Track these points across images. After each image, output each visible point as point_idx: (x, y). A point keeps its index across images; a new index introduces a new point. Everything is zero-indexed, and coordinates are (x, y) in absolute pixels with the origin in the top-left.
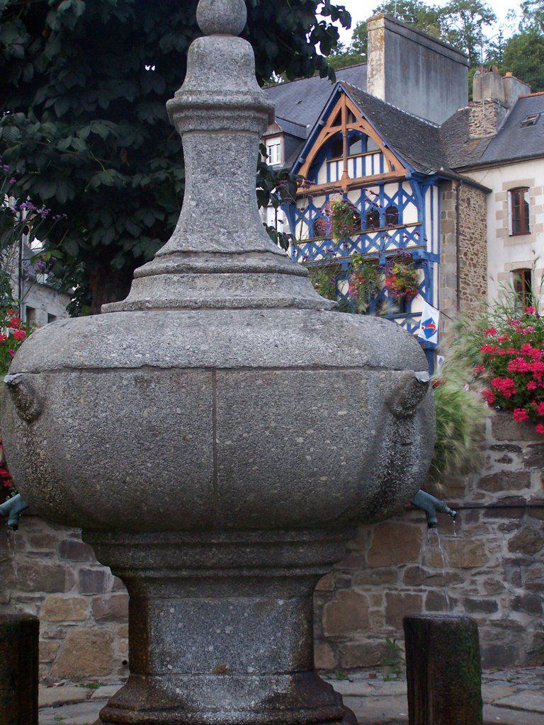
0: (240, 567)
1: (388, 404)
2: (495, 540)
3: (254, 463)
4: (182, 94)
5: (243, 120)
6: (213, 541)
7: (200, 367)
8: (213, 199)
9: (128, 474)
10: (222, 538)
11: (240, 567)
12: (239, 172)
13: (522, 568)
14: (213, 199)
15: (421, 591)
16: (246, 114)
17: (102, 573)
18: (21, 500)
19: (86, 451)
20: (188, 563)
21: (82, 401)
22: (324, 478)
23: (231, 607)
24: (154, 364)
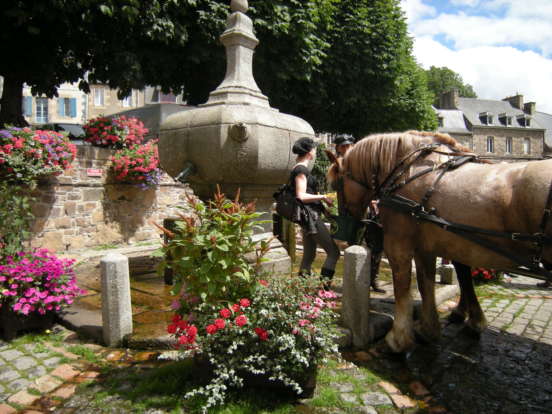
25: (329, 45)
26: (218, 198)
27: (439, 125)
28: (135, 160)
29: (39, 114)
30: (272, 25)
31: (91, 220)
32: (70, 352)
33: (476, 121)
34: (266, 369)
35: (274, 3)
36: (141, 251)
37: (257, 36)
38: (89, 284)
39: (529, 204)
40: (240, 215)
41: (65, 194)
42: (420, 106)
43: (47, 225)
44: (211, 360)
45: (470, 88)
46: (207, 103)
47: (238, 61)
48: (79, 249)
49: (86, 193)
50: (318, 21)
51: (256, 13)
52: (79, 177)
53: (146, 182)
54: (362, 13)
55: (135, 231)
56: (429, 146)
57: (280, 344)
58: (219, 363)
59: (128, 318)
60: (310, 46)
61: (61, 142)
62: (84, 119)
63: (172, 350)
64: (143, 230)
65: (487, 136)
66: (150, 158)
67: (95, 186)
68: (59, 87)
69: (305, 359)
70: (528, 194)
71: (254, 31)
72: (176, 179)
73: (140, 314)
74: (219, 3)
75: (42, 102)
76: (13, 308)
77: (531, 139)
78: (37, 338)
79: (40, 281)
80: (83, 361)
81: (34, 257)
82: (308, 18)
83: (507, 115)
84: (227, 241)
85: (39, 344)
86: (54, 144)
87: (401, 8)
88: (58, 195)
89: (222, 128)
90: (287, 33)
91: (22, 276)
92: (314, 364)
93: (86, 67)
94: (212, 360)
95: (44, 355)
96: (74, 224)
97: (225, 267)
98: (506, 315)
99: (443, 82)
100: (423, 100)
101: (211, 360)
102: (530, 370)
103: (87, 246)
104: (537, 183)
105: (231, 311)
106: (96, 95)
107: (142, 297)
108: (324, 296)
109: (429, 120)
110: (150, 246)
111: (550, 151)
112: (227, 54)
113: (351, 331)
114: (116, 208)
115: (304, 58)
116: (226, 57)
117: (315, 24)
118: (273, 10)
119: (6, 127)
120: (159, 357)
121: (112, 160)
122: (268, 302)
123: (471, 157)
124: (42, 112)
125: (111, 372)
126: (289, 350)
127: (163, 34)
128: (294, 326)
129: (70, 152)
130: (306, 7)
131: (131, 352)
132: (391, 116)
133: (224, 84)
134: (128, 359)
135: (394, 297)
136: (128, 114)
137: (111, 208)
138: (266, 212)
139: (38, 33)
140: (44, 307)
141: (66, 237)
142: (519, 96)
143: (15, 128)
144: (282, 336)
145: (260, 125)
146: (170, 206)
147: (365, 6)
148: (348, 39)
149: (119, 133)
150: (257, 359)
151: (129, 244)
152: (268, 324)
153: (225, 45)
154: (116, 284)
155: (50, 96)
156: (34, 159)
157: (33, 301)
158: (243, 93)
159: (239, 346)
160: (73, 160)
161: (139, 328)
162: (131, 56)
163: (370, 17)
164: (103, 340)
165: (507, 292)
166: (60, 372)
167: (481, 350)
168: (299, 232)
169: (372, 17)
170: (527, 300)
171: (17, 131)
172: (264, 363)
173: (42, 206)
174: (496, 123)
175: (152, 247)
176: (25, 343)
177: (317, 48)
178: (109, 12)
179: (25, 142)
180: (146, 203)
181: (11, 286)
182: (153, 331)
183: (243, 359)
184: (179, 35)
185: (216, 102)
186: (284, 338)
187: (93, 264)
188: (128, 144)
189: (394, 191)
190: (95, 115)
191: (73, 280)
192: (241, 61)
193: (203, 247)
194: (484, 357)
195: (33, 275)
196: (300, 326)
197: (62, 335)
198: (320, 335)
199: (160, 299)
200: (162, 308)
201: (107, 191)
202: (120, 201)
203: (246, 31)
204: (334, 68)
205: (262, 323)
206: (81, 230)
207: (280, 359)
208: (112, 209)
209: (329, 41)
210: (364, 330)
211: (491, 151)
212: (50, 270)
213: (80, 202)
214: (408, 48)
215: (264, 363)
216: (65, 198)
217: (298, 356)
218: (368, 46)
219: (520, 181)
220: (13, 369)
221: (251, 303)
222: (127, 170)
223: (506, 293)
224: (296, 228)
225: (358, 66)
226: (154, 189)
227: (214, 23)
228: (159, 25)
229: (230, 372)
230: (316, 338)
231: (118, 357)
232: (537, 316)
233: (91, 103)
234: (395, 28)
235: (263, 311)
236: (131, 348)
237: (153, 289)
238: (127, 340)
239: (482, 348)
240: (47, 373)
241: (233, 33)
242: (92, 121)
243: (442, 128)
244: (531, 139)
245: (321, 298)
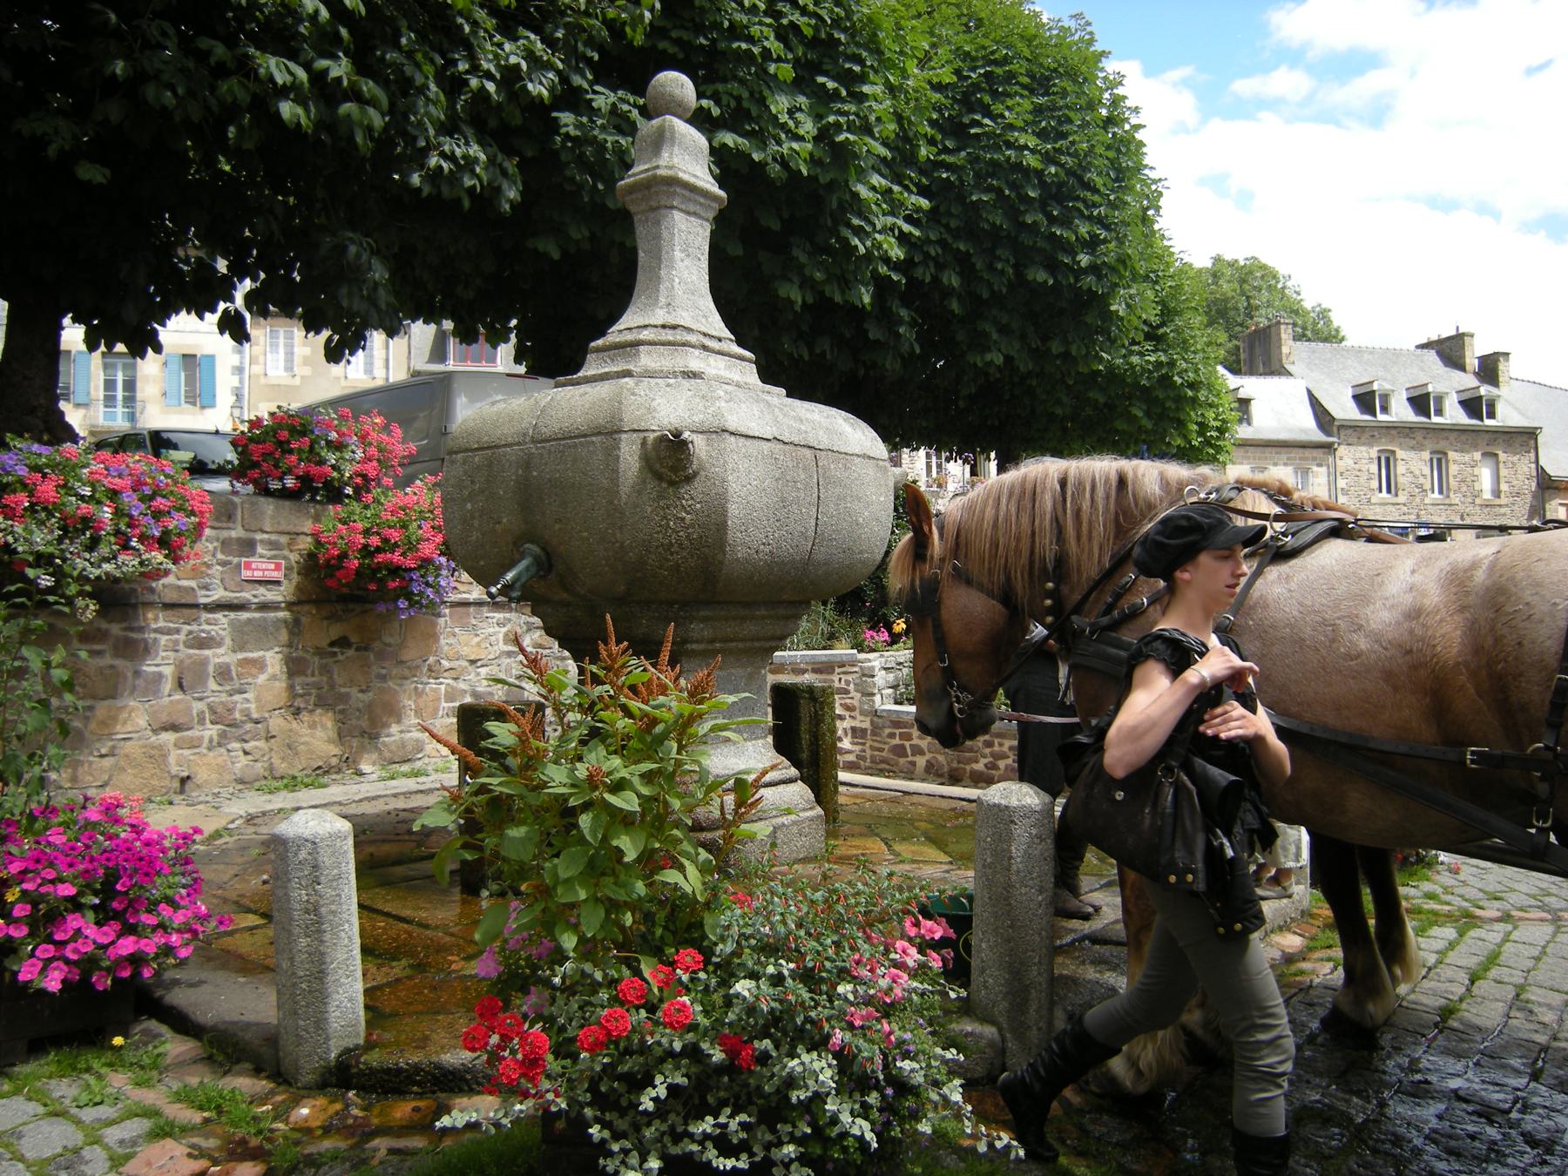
25: (924, 203)
26: (610, 656)
27: (1240, 421)
28: (379, 534)
29: (110, 401)
30: (764, 150)
31: (253, 706)
32: (179, 1101)
33: (1344, 408)
34: (752, 1155)
35: (770, 88)
36: (395, 795)
37: (721, 181)
38: (242, 896)
39: (1510, 659)
40: (672, 704)
41: (178, 631)
42: (1186, 371)
43: (125, 723)
44: (590, 1131)
45: (1324, 314)
46: (580, 374)
47: (667, 253)
48: (216, 791)
49: (239, 630)
50: (893, 136)
51: (718, 118)
52: (218, 582)
53: (409, 596)
54: (1017, 114)
55: (377, 737)
56: (1213, 496)
57: (791, 1082)
58: (617, 1136)
59: (351, 1000)
60: (873, 207)
61: (167, 485)
62: (237, 412)
63: (479, 1093)
64: (401, 732)
65: (1376, 449)
66: (420, 527)
67: (264, 607)
68: (164, 325)
69: (866, 1125)
70: (1505, 631)
71: (713, 167)
72: (493, 590)
73: (388, 984)
74: (614, 90)
75: (120, 366)
76: (15, 974)
77: (1502, 456)
78: (87, 1061)
79: (96, 893)
80: (219, 1130)
81: (82, 822)
82: (866, 129)
83: (1430, 388)
84: (636, 781)
85: (92, 1080)
86: (148, 491)
87: (1125, 97)
88: (158, 636)
89: (623, 445)
90: (805, 173)
91: (43, 879)
92: (894, 1138)
93: (240, 270)
94: (594, 1130)
95: (105, 1111)
96: (204, 719)
97: (631, 855)
98: (1448, 972)
99: (1248, 298)
100: (1194, 352)
101: (590, 1131)
102: (1527, 1142)
103: (241, 781)
104: (1529, 599)
105: (647, 983)
106: (271, 346)
107: (393, 933)
108: (919, 935)
109: (1211, 406)
110: (420, 779)
111: (1556, 488)
112: (638, 232)
113: (1000, 1030)
114: (325, 670)
115: (856, 241)
116: (634, 240)
117: (885, 144)
118: (768, 108)
119: (11, 444)
120: (437, 1124)
121: (312, 535)
122: (756, 957)
123: (1336, 523)
124: (120, 394)
125: (299, 1162)
126: (819, 1098)
127: (453, 178)
128: (833, 1028)
129: (192, 513)
130: (861, 98)
131: (359, 1101)
132: (1102, 400)
133: (629, 319)
134: (350, 1121)
135: (1120, 926)
136: (353, 404)
137: (309, 672)
138: (747, 694)
139: (104, 181)
140: (108, 969)
141: (179, 755)
142: (1463, 334)
143: (36, 447)
144: (799, 1057)
145: (732, 433)
146: (479, 664)
147: (1026, 93)
148: (980, 186)
149: (332, 458)
150: (725, 1126)
151: (362, 774)
152: (756, 1023)
153: (632, 209)
154: (317, 901)
155: (137, 351)
156: (88, 534)
157: (77, 951)
158: (684, 345)
159: (672, 1088)
160: (200, 535)
161: (384, 1030)
162: (361, 244)
163: (1040, 122)
164: (278, 1065)
165: (1448, 904)
166: (149, 1164)
167: (1381, 1081)
168: (846, 735)
169: (1043, 124)
170: (1509, 927)
171: (40, 455)
172: (745, 1136)
173: (112, 667)
174: (1401, 411)
175: (428, 782)
176: (50, 1077)
177: (892, 214)
178: (304, 121)
179: (65, 486)
180: (409, 654)
181: (12, 909)
182: (426, 1039)
183: (686, 1124)
184: (496, 184)
185: (607, 370)
186: (803, 1064)
187: (256, 833)
188: (357, 489)
189: (1115, 626)
190: (269, 401)
191: (195, 888)
192: (678, 254)
193: (564, 798)
194: (1391, 1102)
195: (75, 877)
196: (851, 1027)
197: (161, 1050)
198: (908, 1052)
199: (448, 939)
200: (453, 967)
201: (297, 622)
202: (335, 650)
203: (691, 169)
204: (940, 266)
205: (740, 1019)
206: (223, 735)
207: (794, 1126)
208: (313, 675)
209: (923, 191)
210: (1040, 1029)
211: (1389, 491)
212: (126, 860)
213: (219, 656)
214: (1148, 209)
215: (745, 1136)
216: (176, 642)
217: (846, 1118)
218: (1037, 205)
219: (1482, 593)
220: (9, 1156)
221: (707, 962)
222: (356, 562)
223: (1447, 908)
224: (838, 723)
225: (1007, 261)
226: (433, 615)
227: (601, 147)
228: (443, 155)
229: (646, 1166)
230: (899, 1064)
231: (323, 1116)
232: (1540, 975)
233: (257, 369)
234: (1111, 154)
235: (743, 987)
236: (362, 1089)
237: (427, 909)
238: (349, 1067)
239: (1384, 1077)
240: (111, 1169)
241: (655, 176)
242: (255, 423)
243: (1250, 429)
244: (1502, 456)
245: (910, 940)
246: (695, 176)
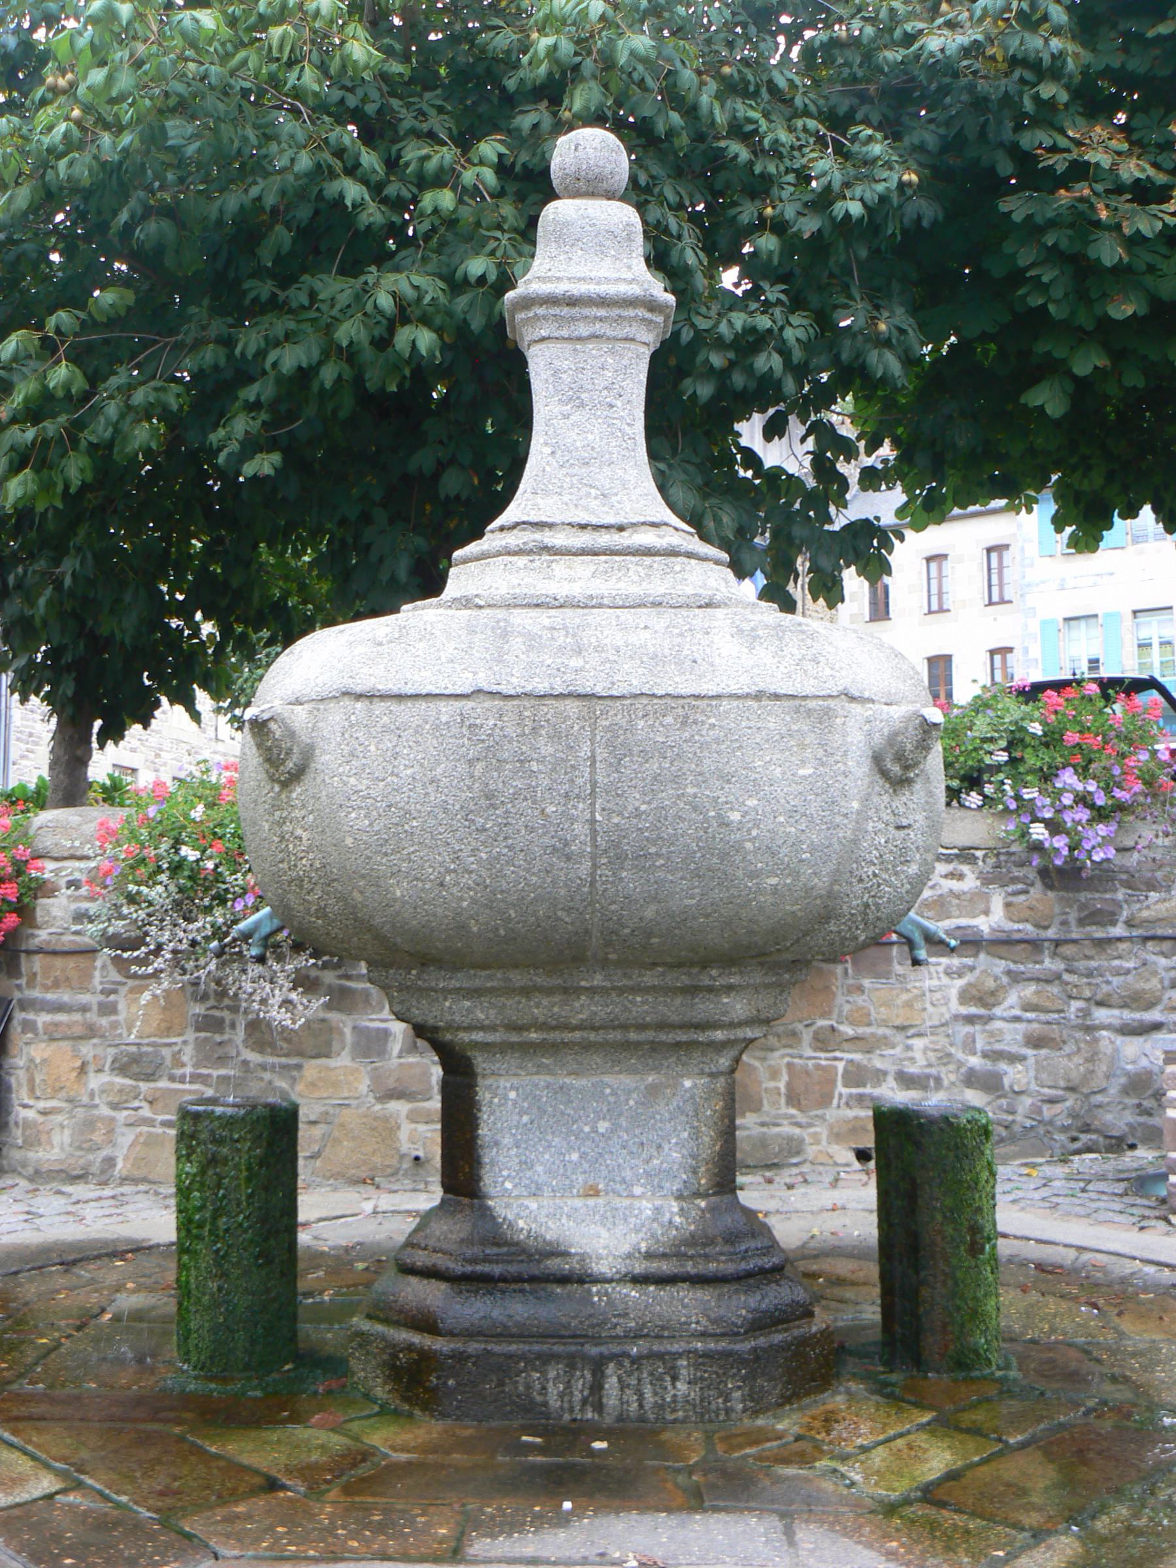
0: (625, 1027)
1: (877, 759)
2: (940, 988)
3: (659, 855)
4: (529, 281)
5: (626, 323)
6: (583, 983)
7: (569, 695)
8: (578, 444)
9: (449, 871)
10: (598, 980)
11: (625, 1027)
12: (619, 404)
13: (978, 1027)
14: (578, 444)
15: (836, 1059)
16: (631, 312)
17: (386, 1033)
18: (271, 916)
19: (377, 833)
20: (541, 1019)
21: (372, 748)
22: (774, 881)
23: (608, 1091)
24: (495, 688)
146: (911, 1032)
246: (607, 280)
